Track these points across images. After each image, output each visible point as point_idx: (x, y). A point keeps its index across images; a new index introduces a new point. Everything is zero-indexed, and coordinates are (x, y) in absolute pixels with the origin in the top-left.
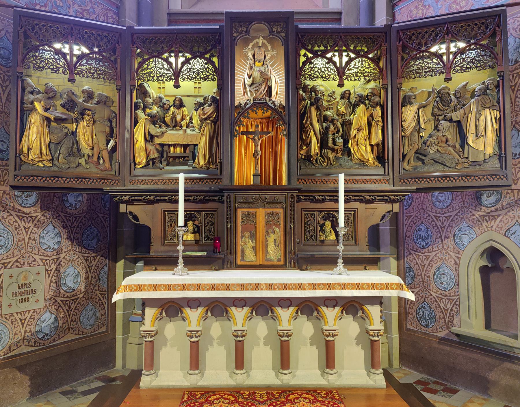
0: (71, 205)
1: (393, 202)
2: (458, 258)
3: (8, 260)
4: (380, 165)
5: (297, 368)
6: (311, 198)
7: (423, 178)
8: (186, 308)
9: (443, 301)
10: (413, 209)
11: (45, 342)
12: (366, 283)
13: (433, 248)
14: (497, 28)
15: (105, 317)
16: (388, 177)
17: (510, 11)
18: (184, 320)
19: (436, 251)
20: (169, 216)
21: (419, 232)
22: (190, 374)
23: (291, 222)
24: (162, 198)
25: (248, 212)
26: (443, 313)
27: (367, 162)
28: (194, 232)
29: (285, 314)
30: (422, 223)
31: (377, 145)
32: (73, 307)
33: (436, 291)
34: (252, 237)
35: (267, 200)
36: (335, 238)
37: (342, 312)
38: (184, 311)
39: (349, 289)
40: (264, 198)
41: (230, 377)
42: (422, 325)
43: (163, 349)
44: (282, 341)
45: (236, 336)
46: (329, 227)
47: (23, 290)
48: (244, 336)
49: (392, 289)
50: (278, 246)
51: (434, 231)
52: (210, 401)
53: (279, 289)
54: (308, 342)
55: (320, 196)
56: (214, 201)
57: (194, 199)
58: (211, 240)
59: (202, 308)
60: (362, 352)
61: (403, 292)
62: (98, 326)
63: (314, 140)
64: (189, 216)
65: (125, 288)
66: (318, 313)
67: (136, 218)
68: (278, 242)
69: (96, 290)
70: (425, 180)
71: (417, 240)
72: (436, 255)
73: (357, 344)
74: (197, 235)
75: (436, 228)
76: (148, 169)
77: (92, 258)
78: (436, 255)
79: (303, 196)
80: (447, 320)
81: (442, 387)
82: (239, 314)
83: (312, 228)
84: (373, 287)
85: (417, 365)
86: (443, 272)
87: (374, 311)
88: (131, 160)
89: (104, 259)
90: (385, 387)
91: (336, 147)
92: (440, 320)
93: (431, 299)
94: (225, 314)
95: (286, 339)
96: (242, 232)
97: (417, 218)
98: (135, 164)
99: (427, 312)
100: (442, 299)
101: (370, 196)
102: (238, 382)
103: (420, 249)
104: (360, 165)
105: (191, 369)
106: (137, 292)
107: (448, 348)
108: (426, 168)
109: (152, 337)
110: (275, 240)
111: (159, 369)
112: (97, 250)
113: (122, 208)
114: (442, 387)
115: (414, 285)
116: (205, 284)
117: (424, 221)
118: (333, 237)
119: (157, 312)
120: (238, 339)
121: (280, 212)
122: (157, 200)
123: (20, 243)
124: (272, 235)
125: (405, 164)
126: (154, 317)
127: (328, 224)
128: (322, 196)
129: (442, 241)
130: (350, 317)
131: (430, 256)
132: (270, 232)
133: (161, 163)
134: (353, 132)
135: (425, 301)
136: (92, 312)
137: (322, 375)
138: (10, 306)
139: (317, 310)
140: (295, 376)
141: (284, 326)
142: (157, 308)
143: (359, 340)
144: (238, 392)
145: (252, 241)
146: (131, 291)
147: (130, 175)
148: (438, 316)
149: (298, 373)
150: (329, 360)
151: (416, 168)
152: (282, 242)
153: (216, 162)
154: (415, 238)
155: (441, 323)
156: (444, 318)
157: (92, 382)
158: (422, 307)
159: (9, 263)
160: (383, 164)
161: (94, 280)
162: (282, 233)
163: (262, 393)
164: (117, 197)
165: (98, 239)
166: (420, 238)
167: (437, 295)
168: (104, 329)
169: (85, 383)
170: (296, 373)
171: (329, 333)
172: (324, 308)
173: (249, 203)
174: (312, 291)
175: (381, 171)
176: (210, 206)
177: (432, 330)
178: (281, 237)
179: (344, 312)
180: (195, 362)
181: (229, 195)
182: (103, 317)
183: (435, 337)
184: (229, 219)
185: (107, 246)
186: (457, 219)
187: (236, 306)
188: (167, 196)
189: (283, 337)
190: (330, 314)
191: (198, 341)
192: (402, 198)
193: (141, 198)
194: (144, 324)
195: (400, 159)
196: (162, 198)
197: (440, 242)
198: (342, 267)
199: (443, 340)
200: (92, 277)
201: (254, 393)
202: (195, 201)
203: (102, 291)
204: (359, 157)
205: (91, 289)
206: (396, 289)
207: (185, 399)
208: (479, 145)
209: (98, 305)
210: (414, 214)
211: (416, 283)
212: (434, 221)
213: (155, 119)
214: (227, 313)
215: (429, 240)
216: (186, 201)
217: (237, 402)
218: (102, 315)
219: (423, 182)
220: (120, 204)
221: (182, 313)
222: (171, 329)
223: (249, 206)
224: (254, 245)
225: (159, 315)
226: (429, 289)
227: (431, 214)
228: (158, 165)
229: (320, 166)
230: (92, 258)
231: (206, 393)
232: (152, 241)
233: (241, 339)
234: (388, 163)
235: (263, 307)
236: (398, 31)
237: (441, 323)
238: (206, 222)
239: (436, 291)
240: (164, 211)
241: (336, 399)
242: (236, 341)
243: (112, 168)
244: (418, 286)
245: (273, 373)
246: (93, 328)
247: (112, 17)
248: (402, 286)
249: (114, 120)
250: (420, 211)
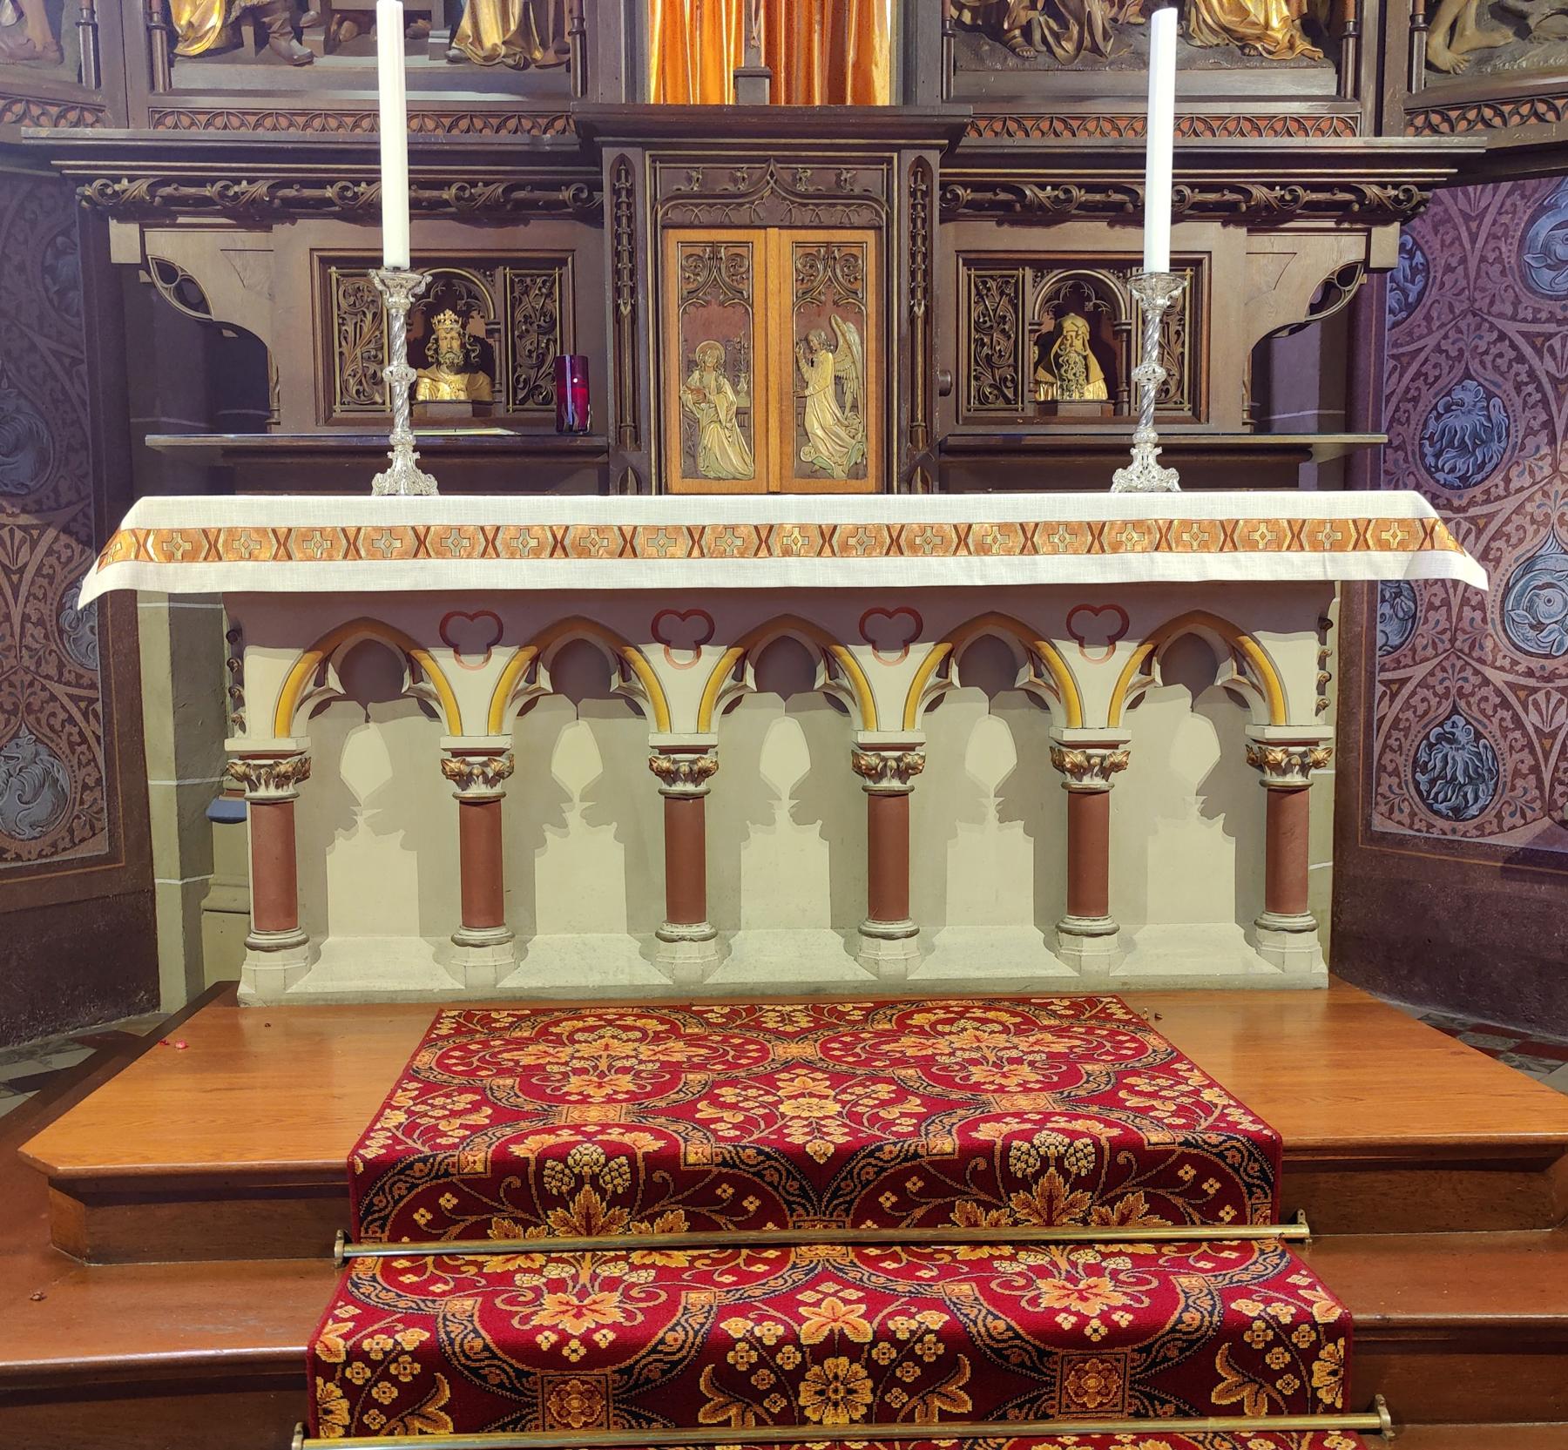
1: (1369, 216)
4: (1319, 53)
5: (940, 920)
6: (1003, 196)
7: (1516, 101)
8: (435, 652)
9: (1536, 703)
10: (1428, 318)
12: (1267, 521)
13: (1507, 480)
15: (98, 798)
16: (1350, 108)
18: (432, 714)
19: (1521, 489)
20: (348, 284)
22: (464, 944)
23: (913, 292)
24: (307, 192)
25: (714, 245)
26: (1533, 751)
27: (1259, 38)
28: (464, 367)
29: (889, 679)
30: (1467, 375)
33: (1507, 663)
34: (735, 367)
35: (801, 188)
36: (1104, 396)
37: (1146, 669)
38: (426, 662)
39: (1188, 548)
40: (787, 176)
41: (644, 955)
42: (1437, 813)
43: (340, 843)
44: (875, 797)
45: (669, 776)
46: (1078, 344)
48: (705, 773)
49: (1384, 546)
50: (854, 407)
51: (1518, 401)
52: (559, 1035)
53: (867, 552)
54: (991, 804)
55: (1042, 187)
56: (553, 210)
57: (458, 198)
58: (547, 401)
59: (513, 650)
60: (1228, 848)
61: (1437, 554)
62: (71, 831)
64: (439, 288)
65: (141, 546)
66: (1038, 675)
67: (189, 291)
68: (851, 387)
69: (47, 677)
70: (1525, 110)
71: (1437, 456)
72: (1522, 506)
73: (1208, 812)
74: (482, 379)
75: (1531, 388)
76: (233, 61)
77: (19, 534)
78: (1518, 510)
79: (965, 186)
80: (1547, 777)
81: (1512, 1043)
82: (682, 679)
83: (1003, 345)
84: (1296, 536)
85: (1404, 972)
86: (1547, 579)
87: (1295, 663)
88: (149, 15)
89: (78, 548)
90: (1325, 982)
92: (1519, 783)
93: (1486, 699)
94: (616, 681)
95: (896, 784)
96: (689, 345)
97: (1442, 359)
98: (173, 38)
99: (1461, 757)
100: (1535, 690)
101: (1271, 186)
102: (682, 974)
103: (1447, 492)
104: (1228, 55)
105: (468, 924)
106: (199, 567)
107: (1543, 890)
108: (1532, 57)
109: (281, 781)
110: (837, 378)
111: (324, 932)
112: (39, 502)
113: (124, 241)
114: (1512, 1043)
115: (1414, 650)
116: (520, 529)
117: (1475, 366)
118: (1096, 390)
119: (301, 667)
120: (679, 787)
121: (859, 244)
122: (286, 201)
124: (827, 360)
125: (1439, 38)
126: (286, 699)
127: (1076, 327)
128: (1055, 187)
129: (1552, 441)
130: (1180, 695)
131: (1490, 517)
132: (815, 342)
133: (298, 34)
135: (1455, 710)
136: (37, 770)
137: (1050, 945)
139: (1037, 659)
140: (929, 949)
141: (888, 727)
142: (298, 652)
143: (1214, 797)
144: (686, 1009)
145: (734, 385)
146: (170, 557)
147: (153, 86)
148: (1510, 766)
149: (944, 937)
150: (1080, 877)
151: (1486, 55)
152: (872, 387)
153: (559, 32)
154: (1428, 450)
155: (1519, 792)
156: (1536, 770)
157: (59, 1052)
158: (1440, 738)
160: (1335, 57)
161: (39, 632)
162: (872, 345)
163: (789, 1008)
164: (90, 180)
166: (1451, 444)
167: (1510, 678)
168: (98, 846)
169: (30, 1054)
170: (936, 940)
171: (1089, 758)
172: (1069, 649)
173: (723, 206)
174: (1016, 559)
175: (1323, 81)
176: (534, 236)
177: (1480, 828)
178: (865, 367)
179: (1156, 669)
180: (486, 889)
181: (622, 160)
182: (87, 796)
183: (1491, 852)
184: (626, 278)
186: (1520, 528)
187: (668, 643)
188: (332, 183)
189: (880, 776)
190: (1095, 674)
191: (496, 800)
192: (1418, 195)
193: (208, 191)
194: (243, 727)
195: (1413, 18)
196: (307, 192)
197: (1545, 450)
198: (1152, 460)
199: (1524, 862)
200: (26, 618)
201: (751, 1011)
202: (471, 214)
203: (79, 686)
204: (1226, 19)
205: (27, 670)
206: (1402, 546)
207: (444, 1032)
209: (64, 745)
210: (1431, 341)
211: (1421, 642)
212: (1521, 359)
214: (625, 676)
215: (1495, 446)
216: (419, 209)
217: (679, 1036)
218: (85, 787)
219: (1516, 119)
220: (113, 223)
221: (417, 676)
222: (370, 754)
223: (716, 216)
224: (745, 403)
225: (310, 687)
226: (1481, 661)
227: (1511, 328)
228: (282, 44)
229: (1044, 59)
230: (19, 534)
231: (535, 1012)
232: (275, 406)
233: (690, 788)
234: (1358, 38)
235: (788, 642)
237: (1519, 792)
238: (519, 317)
239: (1507, 663)
240: (321, 259)
241: (1120, 1021)
242: (668, 797)
243: (60, 49)
244: (1430, 651)
245: (836, 940)
246: (48, 839)
248: (1429, 533)
250: (1463, 325)
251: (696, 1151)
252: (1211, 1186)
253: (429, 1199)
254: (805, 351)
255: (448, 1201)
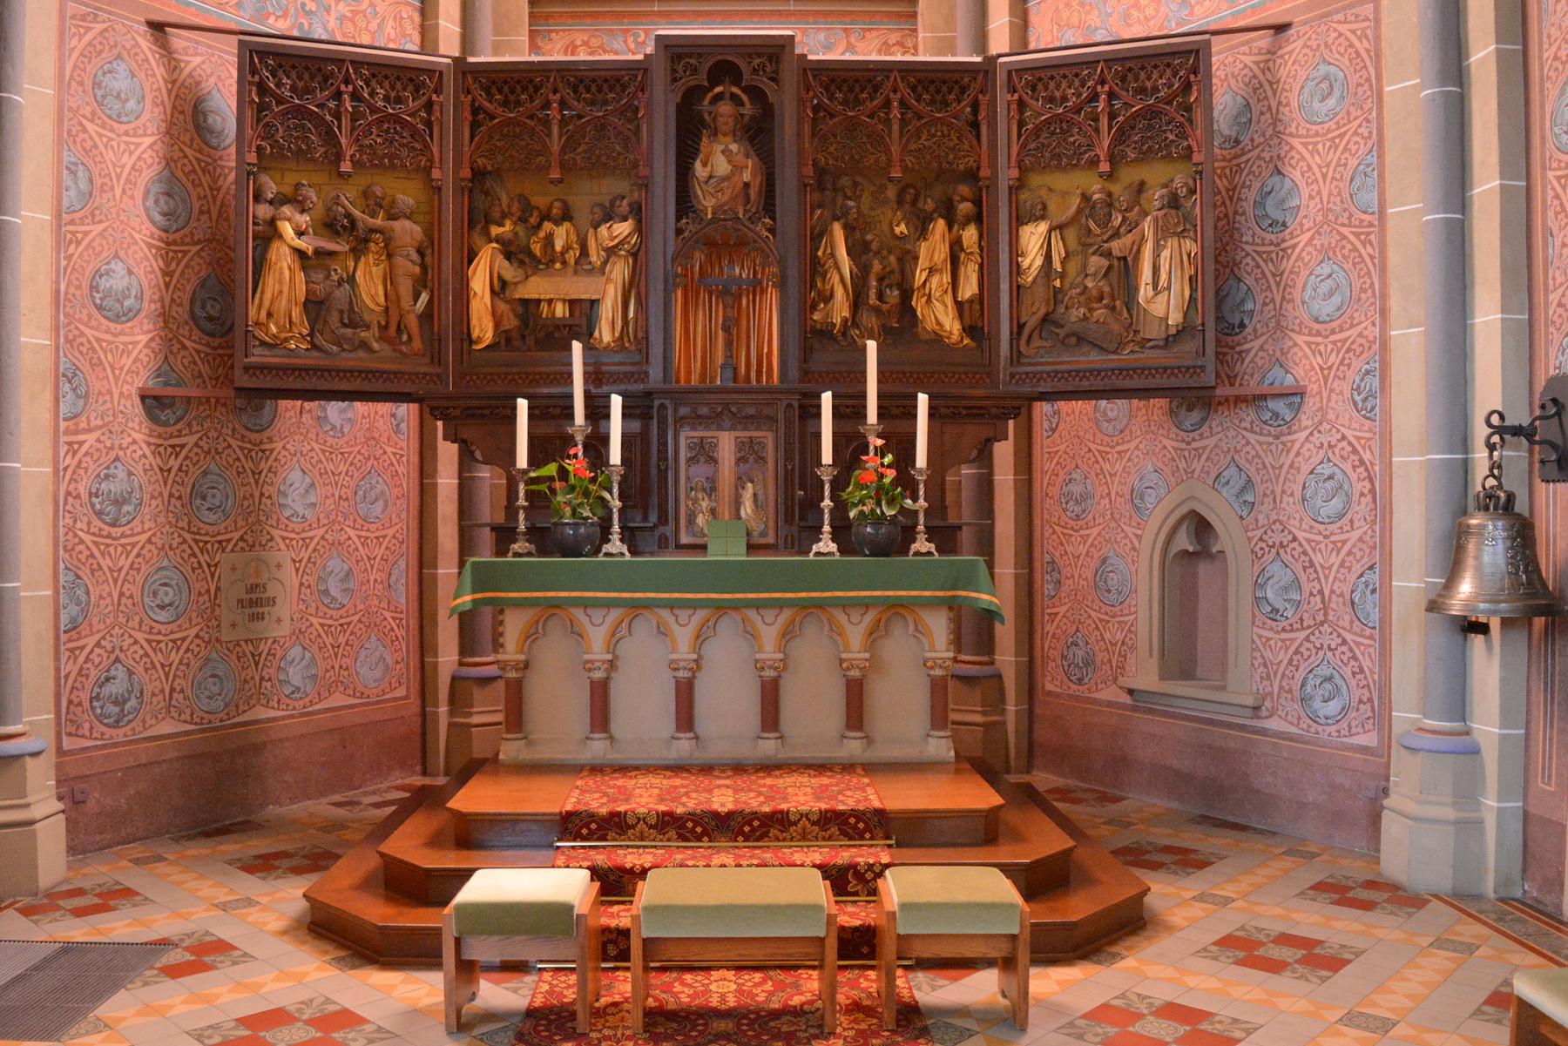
0: (333, 428)
2: (1137, 536)
3: (228, 536)
11: (297, 704)
14: (1192, 77)
17: (1217, 43)
21: (1071, 487)
31: (971, 301)
32: (342, 639)
47: (254, 596)
63: (839, 292)
91: (885, 307)
98: (471, 342)
99: (1080, 653)
123: (246, 503)
134: (920, 277)
138: (234, 625)
156: (1110, 661)
159: (229, 541)
165: (386, 502)
185: (404, 515)
208: (1158, 308)
210: (1062, 448)
213: (512, 249)
227: (1093, 447)
236: (1010, 72)
247: (410, 17)
249: (428, 252)
251: (680, 810)
252: (861, 826)
253: (587, 826)
254: (740, 483)
255: (593, 826)
